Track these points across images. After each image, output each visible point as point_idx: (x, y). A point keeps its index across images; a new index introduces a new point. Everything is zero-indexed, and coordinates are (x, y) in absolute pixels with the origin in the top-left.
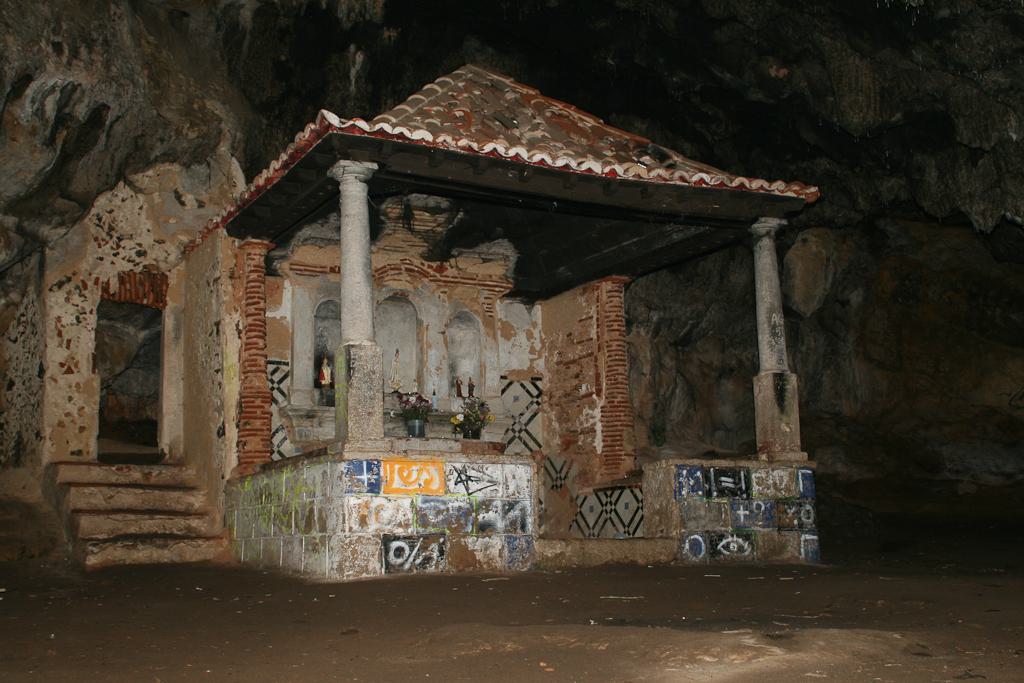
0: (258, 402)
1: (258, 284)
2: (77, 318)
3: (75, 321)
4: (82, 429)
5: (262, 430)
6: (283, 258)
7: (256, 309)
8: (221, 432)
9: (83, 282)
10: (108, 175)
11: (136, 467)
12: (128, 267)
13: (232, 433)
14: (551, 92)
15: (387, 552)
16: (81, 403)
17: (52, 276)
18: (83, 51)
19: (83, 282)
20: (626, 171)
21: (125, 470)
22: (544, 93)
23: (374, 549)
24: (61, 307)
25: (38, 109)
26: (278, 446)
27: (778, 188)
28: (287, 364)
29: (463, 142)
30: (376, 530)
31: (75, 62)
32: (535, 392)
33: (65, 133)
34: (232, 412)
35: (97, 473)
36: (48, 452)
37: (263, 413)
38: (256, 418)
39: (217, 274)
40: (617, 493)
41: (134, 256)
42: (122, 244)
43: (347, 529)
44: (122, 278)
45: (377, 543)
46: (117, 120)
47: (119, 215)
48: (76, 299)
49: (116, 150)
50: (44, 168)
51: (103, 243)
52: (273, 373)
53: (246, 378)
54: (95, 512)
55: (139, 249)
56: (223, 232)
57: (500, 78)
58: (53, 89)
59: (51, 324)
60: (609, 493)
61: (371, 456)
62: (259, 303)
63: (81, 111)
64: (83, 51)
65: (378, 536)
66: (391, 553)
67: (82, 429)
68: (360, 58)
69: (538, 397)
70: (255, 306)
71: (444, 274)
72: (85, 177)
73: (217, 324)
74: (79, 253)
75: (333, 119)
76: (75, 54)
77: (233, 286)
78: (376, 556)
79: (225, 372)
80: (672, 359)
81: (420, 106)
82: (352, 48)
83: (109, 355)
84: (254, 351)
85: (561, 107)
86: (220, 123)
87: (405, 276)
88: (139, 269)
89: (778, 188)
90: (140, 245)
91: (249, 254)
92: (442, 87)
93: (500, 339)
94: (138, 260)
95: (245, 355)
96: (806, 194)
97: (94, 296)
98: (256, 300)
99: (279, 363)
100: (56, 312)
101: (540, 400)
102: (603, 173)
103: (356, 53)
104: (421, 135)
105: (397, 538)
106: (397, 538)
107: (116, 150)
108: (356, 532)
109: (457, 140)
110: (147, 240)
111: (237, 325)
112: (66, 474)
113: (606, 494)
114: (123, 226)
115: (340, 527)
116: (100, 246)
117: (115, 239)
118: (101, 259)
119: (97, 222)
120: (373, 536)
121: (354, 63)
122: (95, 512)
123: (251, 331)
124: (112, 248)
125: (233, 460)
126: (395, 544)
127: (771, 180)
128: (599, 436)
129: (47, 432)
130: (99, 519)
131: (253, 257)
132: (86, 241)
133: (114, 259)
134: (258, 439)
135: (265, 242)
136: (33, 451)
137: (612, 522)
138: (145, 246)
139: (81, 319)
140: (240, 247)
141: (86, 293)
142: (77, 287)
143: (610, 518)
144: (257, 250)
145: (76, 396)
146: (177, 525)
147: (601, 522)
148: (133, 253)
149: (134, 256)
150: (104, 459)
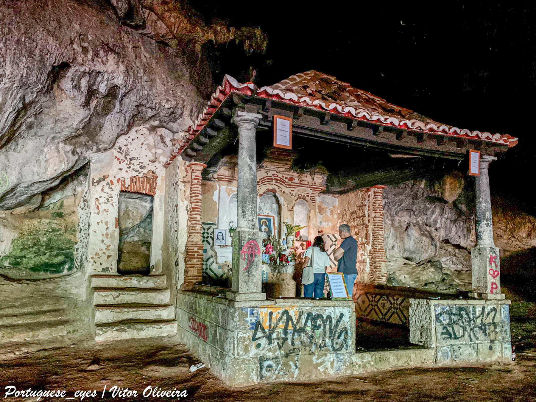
0: (196, 249)
1: (197, 186)
2: (108, 200)
3: (106, 201)
4: (109, 257)
5: (198, 264)
6: (214, 172)
7: (196, 199)
8: (177, 264)
9: (111, 181)
10: (122, 125)
11: (135, 278)
14: (356, 84)
15: (261, 369)
16: (108, 244)
18: (102, 53)
19: (111, 181)
20: (413, 124)
21: (129, 280)
22: (352, 85)
25: (76, 86)
26: (210, 266)
28: (215, 225)
29: (316, 102)
30: (255, 355)
31: (96, 59)
32: (334, 240)
33: (95, 101)
35: (113, 282)
37: (198, 255)
38: (194, 258)
39: (177, 180)
40: (378, 297)
41: (139, 169)
42: (132, 162)
43: (236, 354)
45: (255, 363)
46: (125, 96)
48: (106, 189)
49: (126, 112)
50: (83, 119)
51: (122, 161)
52: (209, 229)
53: (190, 236)
55: (141, 165)
56: (180, 158)
57: (329, 77)
60: (374, 296)
61: (253, 304)
62: (198, 196)
63: (103, 88)
64: (102, 53)
65: (256, 358)
66: (264, 370)
67: (109, 257)
68: (254, 73)
69: (335, 242)
70: (195, 198)
71: (293, 181)
72: (110, 126)
73: (177, 206)
75: (234, 83)
76: (96, 55)
77: (185, 186)
78: (254, 372)
79: (179, 232)
80: (390, 220)
81: (287, 85)
82: (251, 68)
83: (131, 216)
84: (194, 222)
85: (362, 92)
87: (274, 182)
88: (141, 175)
90: (142, 163)
91: (193, 170)
92: (299, 78)
93: (318, 214)
94: (140, 170)
95: (189, 223)
96: (510, 142)
97: (117, 188)
98: (196, 194)
99: (212, 224)
101: (336, 243)
102: (399, 125)
103: (253, 70)
106: (268, 359)
107: (126, 112)
108: (242, 356)
109: (313, 101)
110: (146, 161)
111: (187, 207)
113: (372, 297)
115: (232, 351)
116: (120, 163)
117: (128, 159)
118: (121, 170)
119: (119, 150)
120: (253, 358)
121: (252, 76)
123: (193, 211)
124: (127, 164)
125: (181, 281)
126: (266, 363)
127: (493, 133)
128: (368, 265)
131: (195, 171)
133: (128, 170)
134: (195, 269)
135: (202, 164)
137: (375, 311)
138: (145, 164)
139: (110, 200)
140: (189, 166)
142: (108, 184)
143: (374, 309)
145: (106, 240)
146: (152, 314)
147: (369, 310)
148: (138, 168)
149: (139, 169)
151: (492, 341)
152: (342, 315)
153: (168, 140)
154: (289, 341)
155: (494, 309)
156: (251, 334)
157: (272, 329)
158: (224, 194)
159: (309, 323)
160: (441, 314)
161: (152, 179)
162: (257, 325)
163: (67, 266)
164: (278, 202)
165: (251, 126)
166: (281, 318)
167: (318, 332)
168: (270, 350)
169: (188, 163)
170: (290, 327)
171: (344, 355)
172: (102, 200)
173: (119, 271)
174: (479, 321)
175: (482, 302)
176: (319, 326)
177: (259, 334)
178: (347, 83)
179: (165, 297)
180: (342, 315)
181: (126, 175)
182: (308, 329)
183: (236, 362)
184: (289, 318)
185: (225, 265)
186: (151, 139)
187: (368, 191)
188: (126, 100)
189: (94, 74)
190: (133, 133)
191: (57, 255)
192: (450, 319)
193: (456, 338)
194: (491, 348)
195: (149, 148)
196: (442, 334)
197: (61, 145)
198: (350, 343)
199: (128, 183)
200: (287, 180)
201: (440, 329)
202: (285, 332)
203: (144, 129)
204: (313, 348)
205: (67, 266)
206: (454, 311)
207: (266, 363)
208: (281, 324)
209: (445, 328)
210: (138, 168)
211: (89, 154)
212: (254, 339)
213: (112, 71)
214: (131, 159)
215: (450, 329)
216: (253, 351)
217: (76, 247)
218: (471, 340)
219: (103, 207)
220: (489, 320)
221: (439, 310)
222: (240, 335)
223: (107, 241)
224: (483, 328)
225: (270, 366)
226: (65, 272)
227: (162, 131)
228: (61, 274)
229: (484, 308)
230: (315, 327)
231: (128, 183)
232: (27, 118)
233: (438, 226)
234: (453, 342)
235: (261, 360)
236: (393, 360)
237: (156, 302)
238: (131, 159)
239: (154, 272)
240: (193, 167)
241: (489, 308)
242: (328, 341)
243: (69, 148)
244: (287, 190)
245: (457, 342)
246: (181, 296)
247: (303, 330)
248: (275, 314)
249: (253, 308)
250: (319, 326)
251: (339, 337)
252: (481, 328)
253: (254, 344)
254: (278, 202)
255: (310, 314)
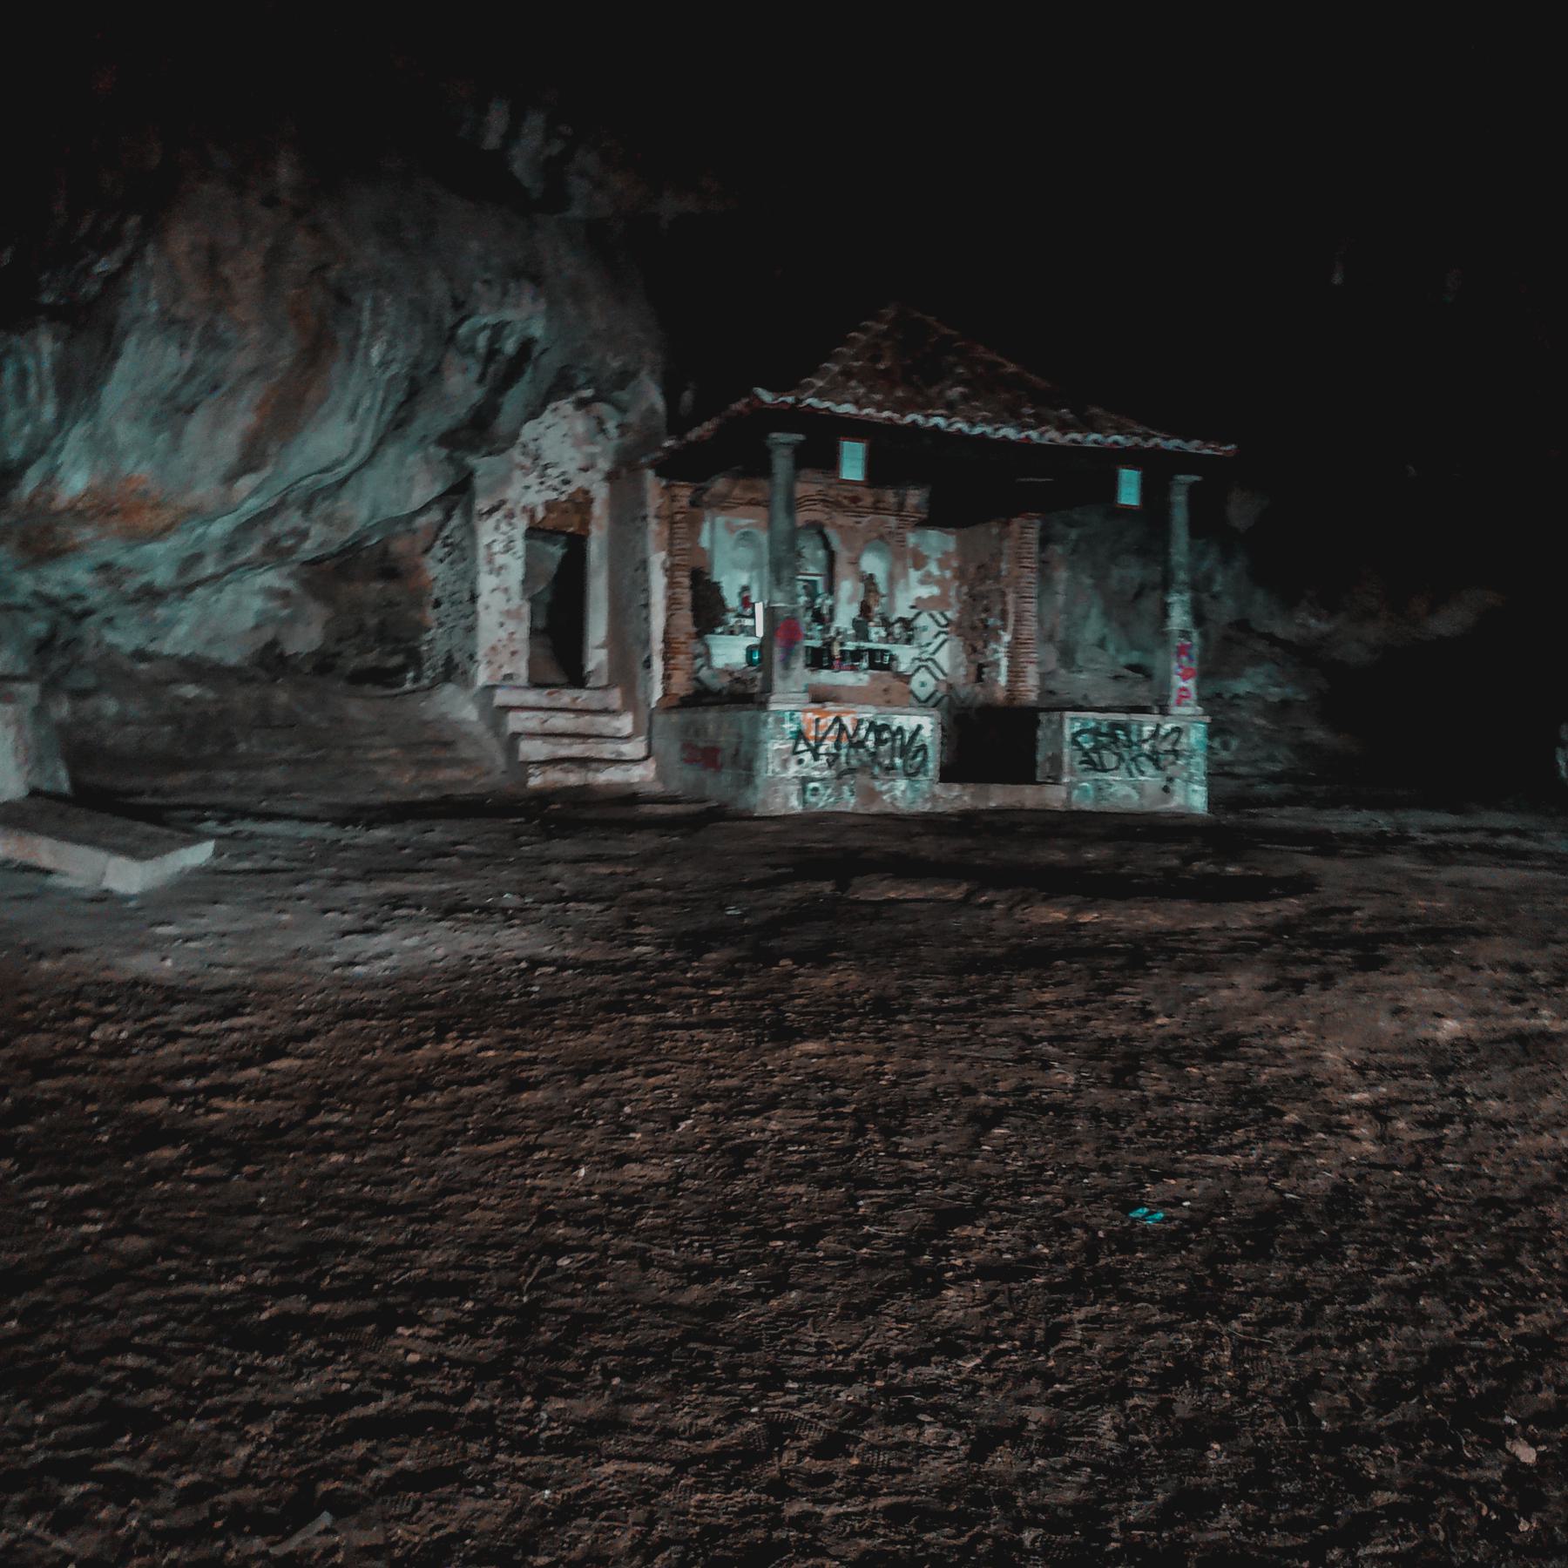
4: (513, 653)
8: (648, 664)
12: (554, 495)
13: (658, 666)
17: (482, 504)
23: (794, 789)
24: (489, 533)
27: (1193, 446)
29: (886, 414)
32: (943, 622)
34: (657, 646)
35: (532, 697)
36: (482, 677)
44: (550, 506)
47: (545, 443)
48: (504, 527)
54: (532, 735)
58: (485, 327)
59: (482, 553)
61: (793, 707)
63: (510, 346)
67: (513, 653)
74: (506, 481)
75: (767, 397)
86: (1139, 1498)
88: (563, 498)
89: (1193, 446)
97: (522, 524)
100: (484, 540)
104: (848, 409)
105: (813, 780)
106: (813, 780)
110: (571, 468)
112: (501, 697)
114: (548, 457)
118: (527, 487)
122: (532, 735)
125: (657, 693)
126: (812, 785)
129: (480, 656)
130: (538, 743)
132: (511, 470)
136: (465, 673)
141: (514, 521)
144: (684, 493)
150: (535, 684)
151: (1170, 779)
152: (919, 727)
153: (611, 426)
154: (843, 759)
155: (1177, 730)
156: (790, 745)
157: (819, 741)
158: (721, 532)
159: (872, 736)
160: (1079, 733)
161: (582, 503)
162: (800, 735)
163: (411, 675)
164: (826, 545)
165: (787, 452)
166: (831, 728)
167: (882, 748)
168: (815, 769)
169: (664, 483)
170: (845, 743)
171: (923, 782)
172: (497, 547)
173: (530, 680)
174: (1146, 747)
175: (1156, 718)
176: (886, 741)
177: (802, 747)
178: (417, 1413)
179: (625, 723)
180: (919, 727)
181: (537, 498)
182: (870, 744)
183: (773, 784)
184: (843, 728)
185: (728, 671)
186: (580, 425)
187: (1008, 524)
188: (545, 360)
189: (498, 330)
190: (547, 417)
191: (393, 653)
192: (1096, 741)
193: (1105, 770)
194: (1166, 789)
195: (577, 444)
196: (1082, 762)
197: (432, 449)
198: (931, 766)
199: (540, 514)
200: (846, 502)
201: (1079, 756)
202: (837, 746)
203: (566, 406)
204: (877, 770)
205: (411, 675)
206: (1104, 730)
207: (812, 785)
208: (831, 734)
209: (1086, 754)
210: (556, 482)
211: (473, 461)
212: (795, 752)
213: (526, 318)
214: (546, 467)
215: (1095, 756)
216: (793, 769)
217: (428, 636)
218: (1131, 775)
219: (500, 560)
220: (1166, 746)
221: (1077, 727)
222: (777, 746)
223: (511, 626)
224: (1154, 758)
225: (815, 789)
226: (408, 686)
227: (602, 408)
228: (396, 691)
229: (1158, 726)
230: (879, 742)
231: (540, 514)
232: (372, 405)
233: (1217, 588)
234: (1099, 775)
235: (805, 781)
236: (998, 796)
237: (607, 731)
238: (546, 467)
239: (592, 683)
240: (677, 491)
241: (1168, 727)
242: (898, 761)
243: (444, 452)
244: (847, 521)
245: (1108, 777)
246: (660, 719)
247: (861, 744)
248: (822, 722)
249: (792, 712)
250: (886, 741)
251: (914, 757)
252: (1149, 758)
253: (794, 759)
254: (826, 545)
255: (872, 724)
